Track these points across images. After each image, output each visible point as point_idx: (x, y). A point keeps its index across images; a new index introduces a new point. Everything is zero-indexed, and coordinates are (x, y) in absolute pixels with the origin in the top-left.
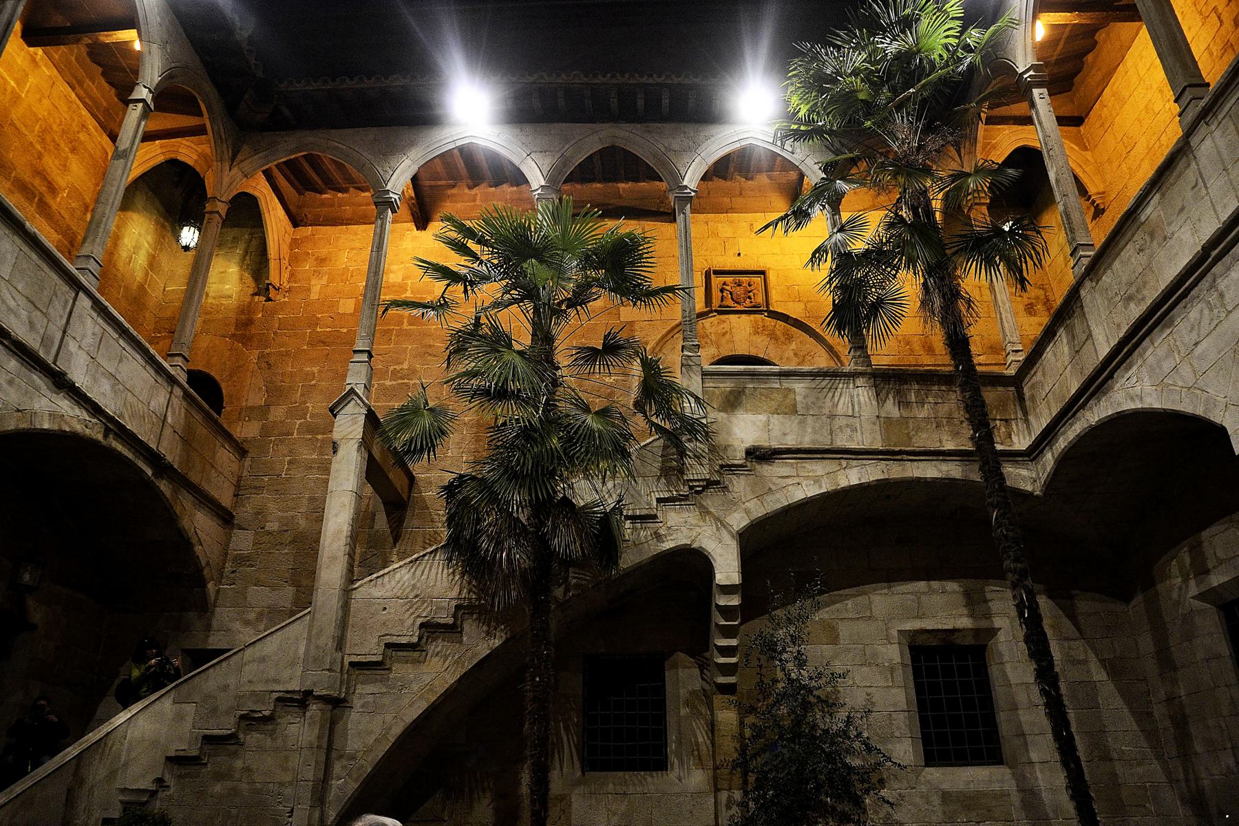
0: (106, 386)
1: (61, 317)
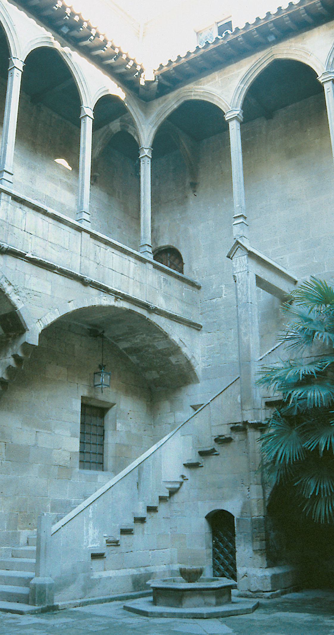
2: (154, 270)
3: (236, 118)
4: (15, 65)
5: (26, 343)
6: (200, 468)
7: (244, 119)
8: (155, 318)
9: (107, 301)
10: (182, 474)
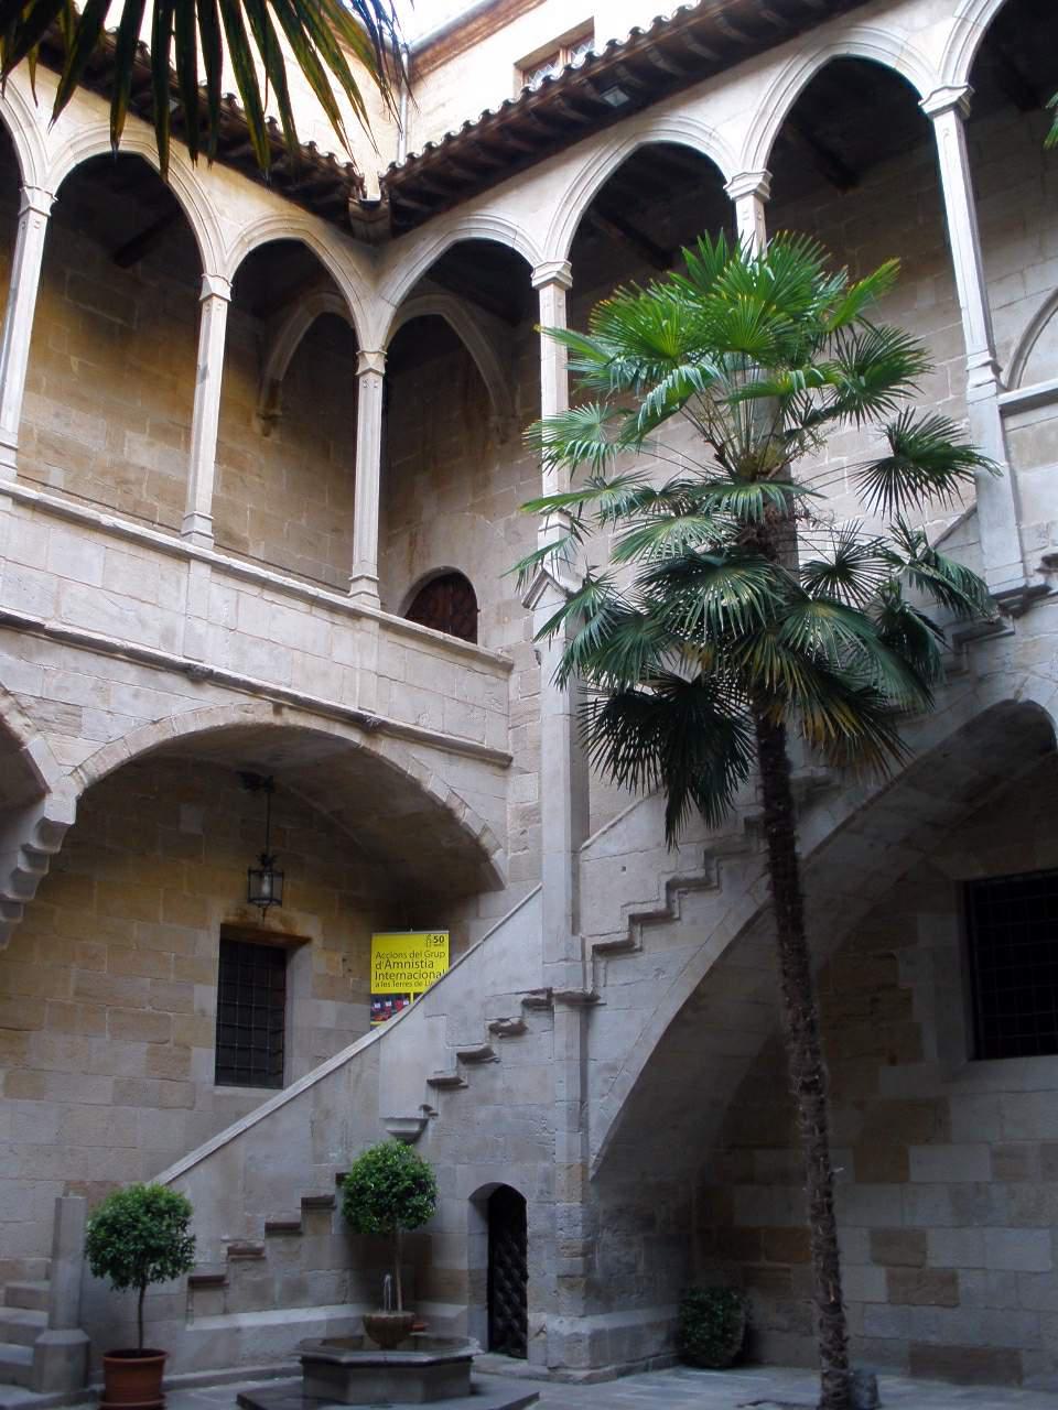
0: (260, 655)
1: (177, 599)
2: (381, 632)
3: (554, 281)
4: (32, 205)
5: (45, 820)
6: (463, 1091)
7: (972, 113)
8: (385, 749)
9: (262, 713)
10: (424, 1103)
